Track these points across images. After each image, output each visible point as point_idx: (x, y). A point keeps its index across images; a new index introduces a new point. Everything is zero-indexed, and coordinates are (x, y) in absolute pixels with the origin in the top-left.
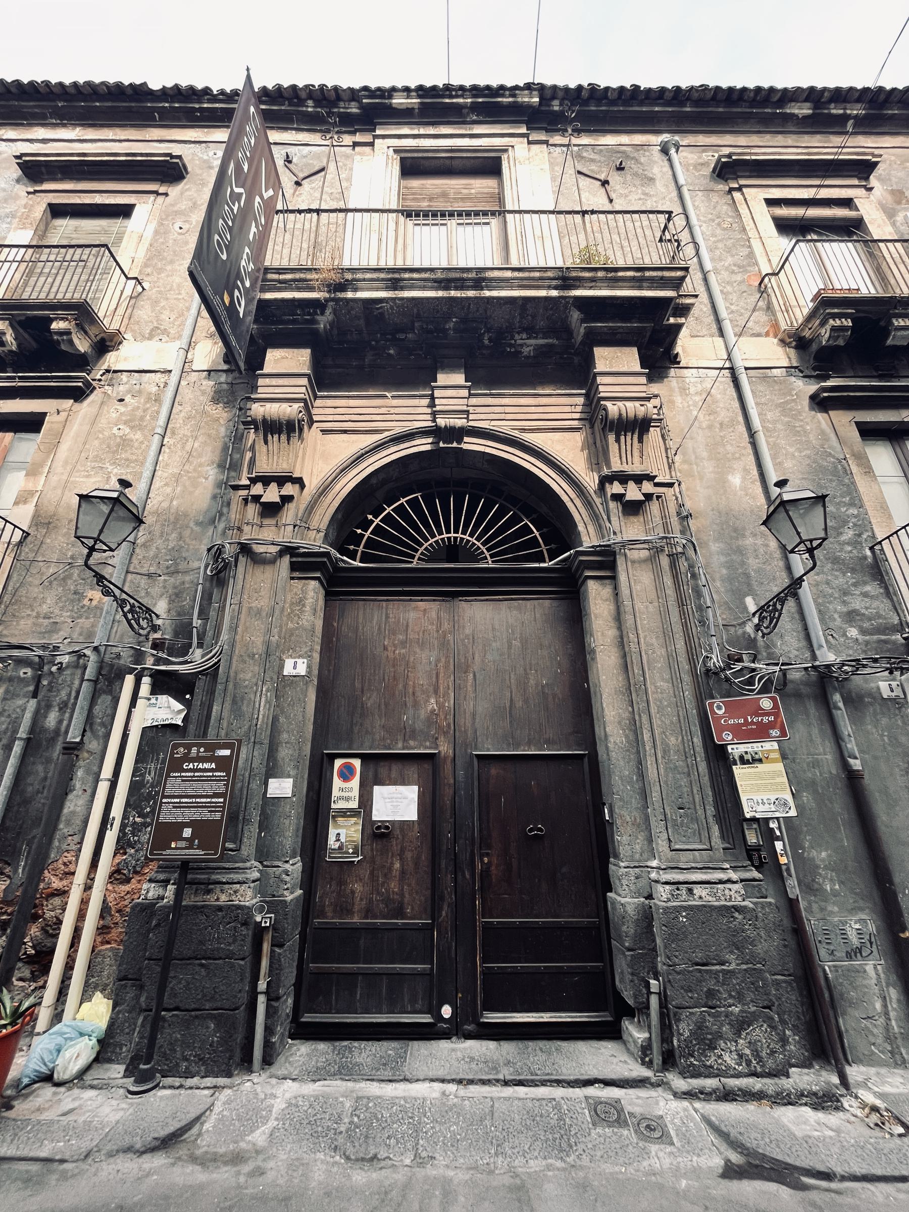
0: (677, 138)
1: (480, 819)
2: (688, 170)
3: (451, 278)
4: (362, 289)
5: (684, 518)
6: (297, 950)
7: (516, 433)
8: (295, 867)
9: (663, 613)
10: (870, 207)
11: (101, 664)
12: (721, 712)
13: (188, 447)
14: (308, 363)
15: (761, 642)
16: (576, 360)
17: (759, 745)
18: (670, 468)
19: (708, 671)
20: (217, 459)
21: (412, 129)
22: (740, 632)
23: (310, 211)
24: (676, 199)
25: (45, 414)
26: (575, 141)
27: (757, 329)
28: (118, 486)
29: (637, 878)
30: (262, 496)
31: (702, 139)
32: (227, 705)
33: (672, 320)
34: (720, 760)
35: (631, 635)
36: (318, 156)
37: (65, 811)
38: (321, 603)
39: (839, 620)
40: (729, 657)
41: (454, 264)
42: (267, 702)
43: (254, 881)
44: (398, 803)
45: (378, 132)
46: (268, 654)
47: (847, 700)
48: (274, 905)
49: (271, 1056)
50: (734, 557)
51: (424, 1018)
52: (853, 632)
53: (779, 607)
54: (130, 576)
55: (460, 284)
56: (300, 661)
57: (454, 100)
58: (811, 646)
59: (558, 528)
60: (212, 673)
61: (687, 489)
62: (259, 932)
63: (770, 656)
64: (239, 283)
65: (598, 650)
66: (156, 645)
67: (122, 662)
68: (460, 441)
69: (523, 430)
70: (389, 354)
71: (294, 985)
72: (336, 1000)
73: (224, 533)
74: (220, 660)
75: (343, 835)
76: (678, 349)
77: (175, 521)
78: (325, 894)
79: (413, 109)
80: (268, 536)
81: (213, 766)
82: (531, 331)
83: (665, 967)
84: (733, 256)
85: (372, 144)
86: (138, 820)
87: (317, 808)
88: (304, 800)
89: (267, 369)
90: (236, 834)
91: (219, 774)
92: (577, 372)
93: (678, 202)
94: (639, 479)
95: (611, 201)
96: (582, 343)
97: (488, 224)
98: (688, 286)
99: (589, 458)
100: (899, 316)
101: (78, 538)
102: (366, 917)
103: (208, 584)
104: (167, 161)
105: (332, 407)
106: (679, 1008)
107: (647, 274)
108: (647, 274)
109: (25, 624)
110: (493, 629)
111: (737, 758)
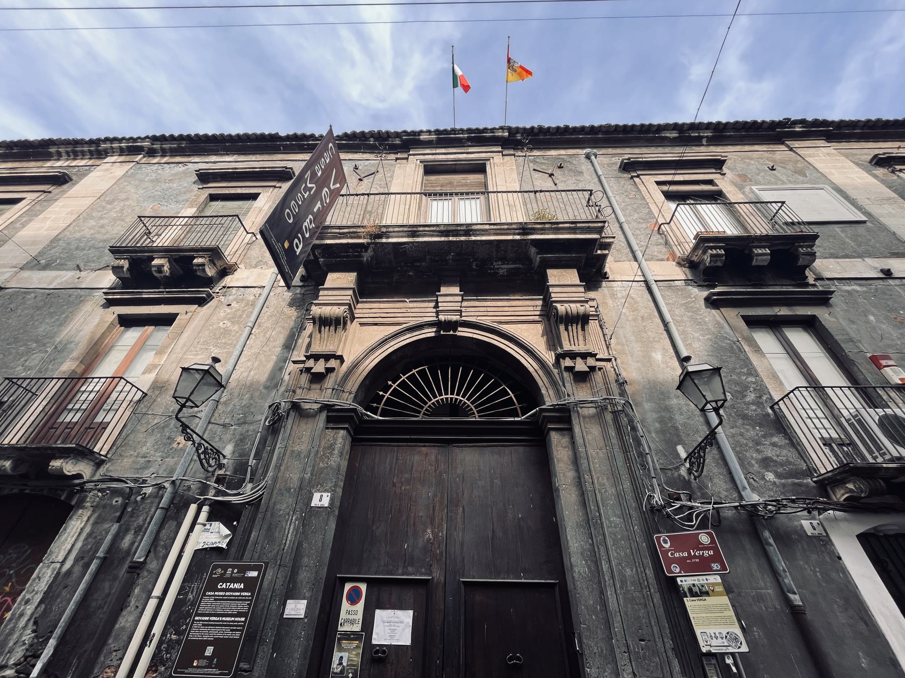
3: (448, 230)
4: (392, 237)
5: (621, 384)
7: (495, 325)
9: (611, 458)
10: (725, 183)
11: (175, 494)
12: (667, 546)
13: (268, 335)
15: (694, 484)
16: (536, 277)
17: (704, 578)
18: (608, 348)
19: (652, 508)
22: (676, 474)
23: (363, 194)
25: (178, 314)
26: (528, 154)
27: (661, 256)
28: (210, 361)
31: (610, 151)
32: (263, 532)
33: (599, 252)
34: (673, 594)
36: (373, 165)
37: (117, 626)
38: (347, 447)
39: (756, 465)
40: (670, 496)
44: (395, 627)
46: (300, 488)
47: (777, 537)
50: (663, 414)
52: (770, 476)
53: (702, 454)
54: (210, 426)
55: (456, 233)
56: (325, 495)
58: (737, 487)
60: (255, 504)
63: (704, 495)
66: (219, 480)
67: (191, 493)
68: (455, 330)
69: (501, 323)
76: (607, 269)
77: (250, 387)
80: (314, 397)
82: (504, 260)
85: (407, 159)
86: (174, 637)
89: (326, 286)
91: (246, 594)
92: (536, 285)
94: (584, 356)
96: (539, 266)
98: (607, 232)
100: (757, 247)
101: (175, 397)
105: (368, 309)
107: (579, 225)
108: (579, 225)
109: (127, 462)
110: (479, 470)
111: (686, 590)
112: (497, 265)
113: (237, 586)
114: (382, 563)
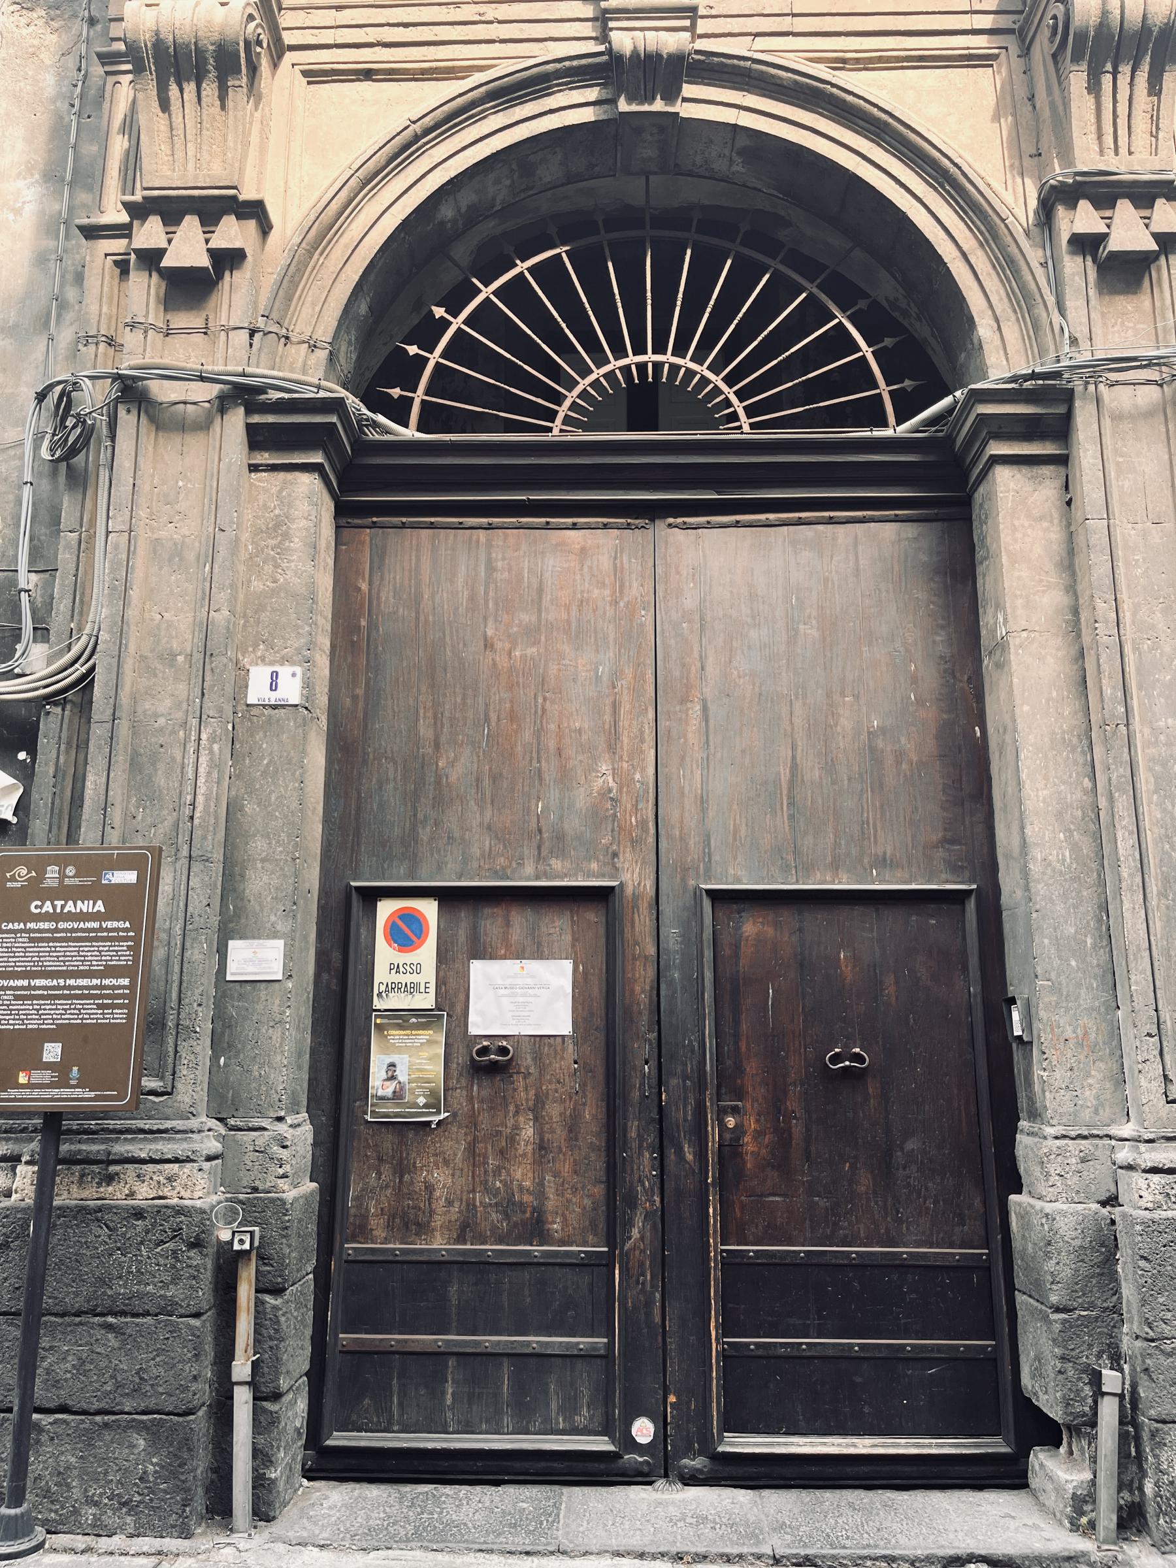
1: (718, 1033)
6: (311, 1304)
7: (821, 71)
8: (299, 1134)
20: (39, 159)
29: (1084, 1160)
30: (164, 251)
35: (1100, 605)
42: (213, 764)
43: (209, 1158)
44: (529, 996)
46: (207, 653)
48: (254, 1206)
49: (270, 1504)
51: (594, 1442)
56: (285, 671)
59: (922, 326)
60: (78, 694)
62: (228, 1266)
65: (1013, 642)
68: (671, 95)
69: (841, 63)
71: (306, 1374)
72: (401, 1404)
73: (74, 354)
74: (93, 669)
75: (404, 1068)
78: (368, 1190)
80: (192, 355)
81: (100, 906)
83: (1139, 1344)
87: (341, 1011)
88: (311, 988)
90: (162, 1057)
91: (115, 924)
99: (1015, 143)
102: (461, 1239)
103: (45, 485)
106: (1164, 1422)
110: (752, 596)
113: (83, 906)
114: (476, 851)
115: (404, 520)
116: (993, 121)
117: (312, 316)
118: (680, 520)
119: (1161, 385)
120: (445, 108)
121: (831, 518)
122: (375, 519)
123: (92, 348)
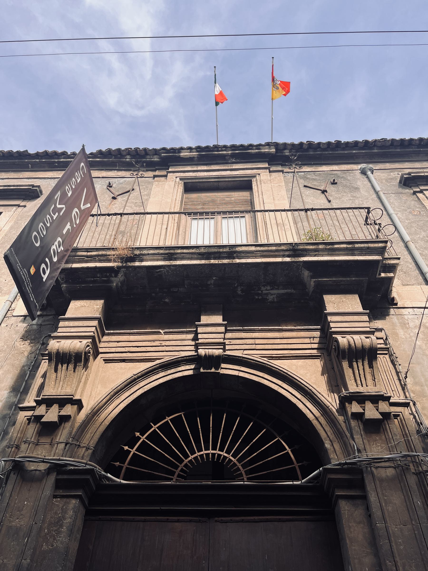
0: (371, 166)
2: (382, 183)
4: (147, 260)
7: (265, 361)
14: (100, 310)
18: (403, 389)
21: (192, 167)
23: (116, 214)
24: (376, 199)
30: (43, 416)
33: (383, 275)
38: (79, 523)
41: (220, 243)
45: (170, 170)
55: (218, 255)
57: (220, 153)
61: (423, 408)
64: (47, 260)
68: (218, 367)
70: (165, 302)
76: (394, 294)
79: (194, 157)
82: (274, 284)
84: (424, 231)
85: (166, 176)
89: (68, 315)
93: (378, 200)
94: (375, 399)
95: (330, 201)
96: (313, 292)
97: (244, 217)
98: (390, 252)
104: (30, 189)
105: (111, 343)
108: (357, 246)
112: (265, 290)
115: (112, 517)
116: (321, 375)
117: (90, 438)
118: (220, 519)
119: (395, 468)
120: (146, 371)
121: (280, 519)
122: (100, 517)
123: (10, 449)
